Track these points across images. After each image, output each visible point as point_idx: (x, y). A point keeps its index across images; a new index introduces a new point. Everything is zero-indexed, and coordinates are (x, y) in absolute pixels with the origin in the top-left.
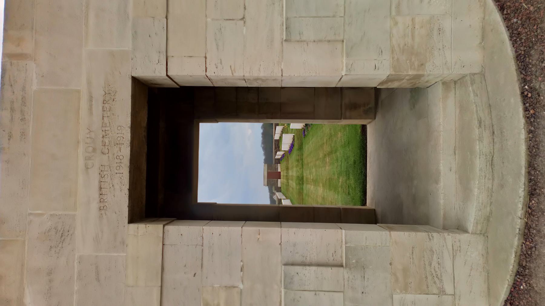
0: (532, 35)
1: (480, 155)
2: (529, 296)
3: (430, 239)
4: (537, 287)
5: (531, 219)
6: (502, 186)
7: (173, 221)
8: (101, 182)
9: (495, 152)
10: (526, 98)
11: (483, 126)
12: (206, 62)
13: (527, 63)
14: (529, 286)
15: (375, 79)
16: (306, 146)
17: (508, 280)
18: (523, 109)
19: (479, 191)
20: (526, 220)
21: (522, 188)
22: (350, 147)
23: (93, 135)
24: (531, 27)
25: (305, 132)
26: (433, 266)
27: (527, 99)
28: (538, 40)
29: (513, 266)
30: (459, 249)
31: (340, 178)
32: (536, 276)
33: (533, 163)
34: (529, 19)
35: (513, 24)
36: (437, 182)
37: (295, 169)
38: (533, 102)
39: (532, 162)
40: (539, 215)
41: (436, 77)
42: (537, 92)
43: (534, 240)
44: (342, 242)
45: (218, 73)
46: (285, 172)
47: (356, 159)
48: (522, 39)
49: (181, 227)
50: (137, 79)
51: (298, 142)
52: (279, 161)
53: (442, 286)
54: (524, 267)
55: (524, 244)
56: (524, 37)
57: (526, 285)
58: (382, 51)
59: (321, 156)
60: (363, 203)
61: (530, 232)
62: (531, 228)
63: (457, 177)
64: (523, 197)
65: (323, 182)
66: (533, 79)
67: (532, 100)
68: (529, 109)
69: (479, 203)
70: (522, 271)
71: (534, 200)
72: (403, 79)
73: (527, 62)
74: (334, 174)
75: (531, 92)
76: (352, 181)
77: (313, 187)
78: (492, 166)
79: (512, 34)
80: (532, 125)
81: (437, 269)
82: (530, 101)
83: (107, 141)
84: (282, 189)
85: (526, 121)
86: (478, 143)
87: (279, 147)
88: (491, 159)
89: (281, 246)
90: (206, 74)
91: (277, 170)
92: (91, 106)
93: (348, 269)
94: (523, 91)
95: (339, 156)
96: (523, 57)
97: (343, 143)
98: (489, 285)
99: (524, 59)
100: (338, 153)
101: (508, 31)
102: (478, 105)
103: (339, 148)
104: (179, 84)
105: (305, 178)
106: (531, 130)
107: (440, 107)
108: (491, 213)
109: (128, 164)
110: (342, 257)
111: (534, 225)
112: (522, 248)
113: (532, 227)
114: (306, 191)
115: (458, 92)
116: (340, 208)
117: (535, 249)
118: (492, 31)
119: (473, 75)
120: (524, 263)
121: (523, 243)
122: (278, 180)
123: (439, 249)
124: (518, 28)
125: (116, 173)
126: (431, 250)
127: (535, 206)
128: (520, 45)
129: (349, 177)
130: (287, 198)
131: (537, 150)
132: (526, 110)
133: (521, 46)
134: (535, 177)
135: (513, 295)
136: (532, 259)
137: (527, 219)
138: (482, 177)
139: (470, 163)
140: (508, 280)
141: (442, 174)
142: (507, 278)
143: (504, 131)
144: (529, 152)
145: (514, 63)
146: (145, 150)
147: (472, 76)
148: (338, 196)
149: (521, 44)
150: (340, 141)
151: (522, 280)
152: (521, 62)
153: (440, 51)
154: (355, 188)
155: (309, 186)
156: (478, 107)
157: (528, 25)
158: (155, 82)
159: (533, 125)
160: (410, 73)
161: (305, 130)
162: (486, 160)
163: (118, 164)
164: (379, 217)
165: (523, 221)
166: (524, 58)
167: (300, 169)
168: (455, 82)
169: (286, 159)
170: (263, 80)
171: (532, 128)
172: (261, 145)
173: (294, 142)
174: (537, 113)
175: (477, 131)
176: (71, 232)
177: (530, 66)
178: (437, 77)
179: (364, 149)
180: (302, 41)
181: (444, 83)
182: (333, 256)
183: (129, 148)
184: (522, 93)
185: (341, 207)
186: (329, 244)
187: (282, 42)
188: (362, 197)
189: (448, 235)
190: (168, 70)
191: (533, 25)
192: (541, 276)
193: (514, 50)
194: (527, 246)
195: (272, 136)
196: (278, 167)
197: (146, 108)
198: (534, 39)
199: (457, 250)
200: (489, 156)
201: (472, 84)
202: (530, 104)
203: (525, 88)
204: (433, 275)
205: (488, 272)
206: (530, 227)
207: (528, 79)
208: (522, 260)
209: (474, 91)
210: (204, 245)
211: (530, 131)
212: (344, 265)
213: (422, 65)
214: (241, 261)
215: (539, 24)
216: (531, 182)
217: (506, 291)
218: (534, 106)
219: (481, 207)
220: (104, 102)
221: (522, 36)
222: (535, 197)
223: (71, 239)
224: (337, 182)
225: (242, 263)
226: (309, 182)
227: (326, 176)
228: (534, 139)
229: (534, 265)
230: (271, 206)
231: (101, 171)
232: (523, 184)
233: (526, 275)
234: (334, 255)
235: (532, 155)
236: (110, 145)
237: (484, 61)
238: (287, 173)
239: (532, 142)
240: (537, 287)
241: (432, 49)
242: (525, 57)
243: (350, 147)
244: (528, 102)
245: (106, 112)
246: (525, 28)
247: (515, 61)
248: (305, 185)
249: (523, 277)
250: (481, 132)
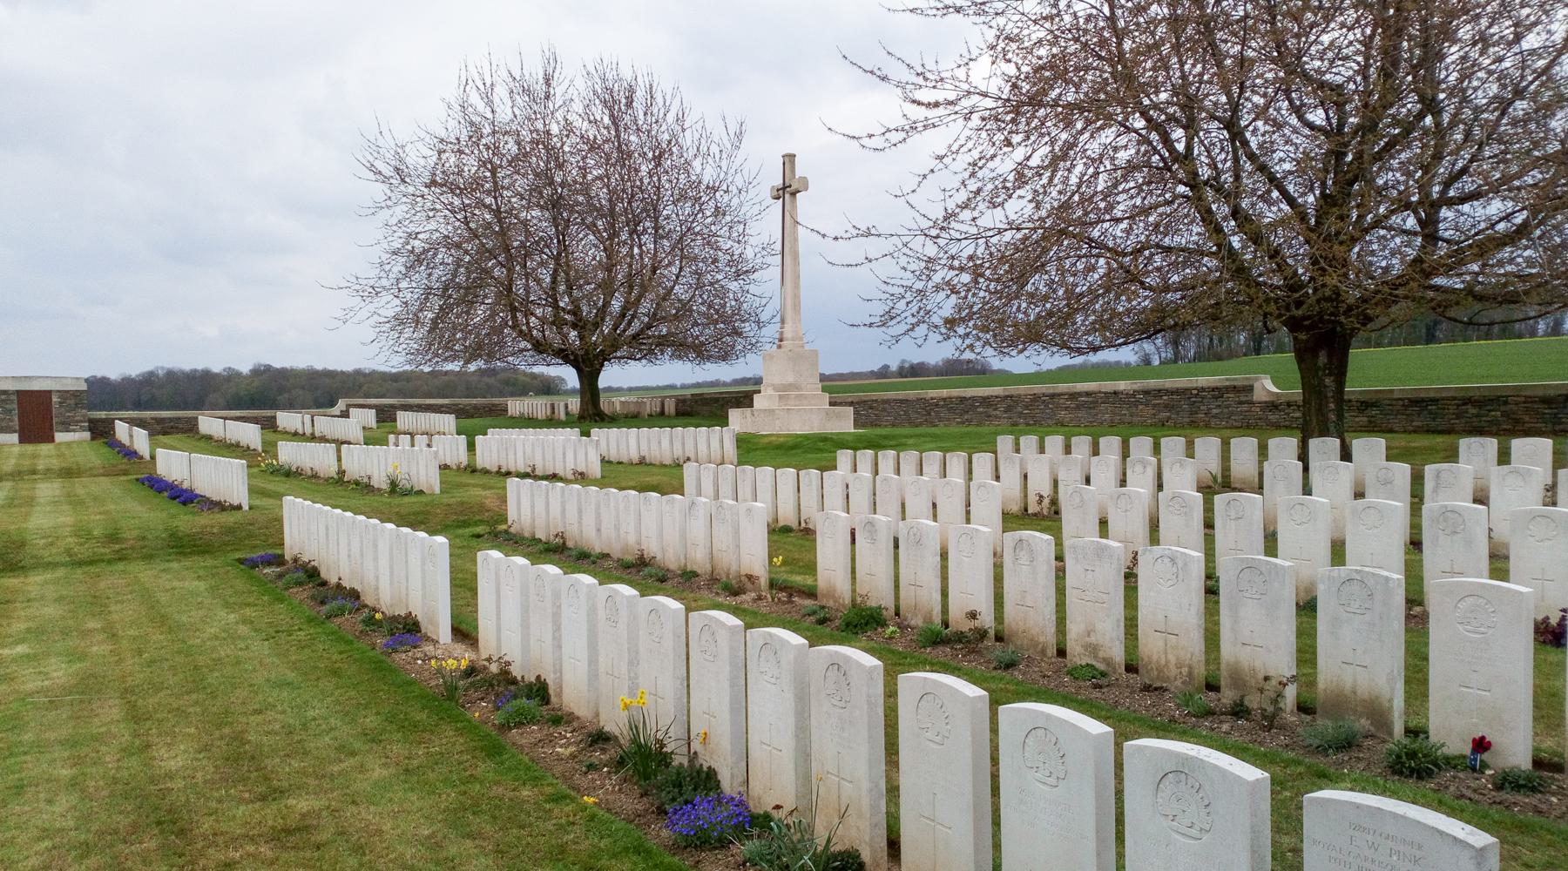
46: (55, 463)
51: (215, 531)
52: (101, 431)
122: (15, 432)
167: (68, 552)
169: (114, 466)
172: (162, 368)
196: (74, 431)
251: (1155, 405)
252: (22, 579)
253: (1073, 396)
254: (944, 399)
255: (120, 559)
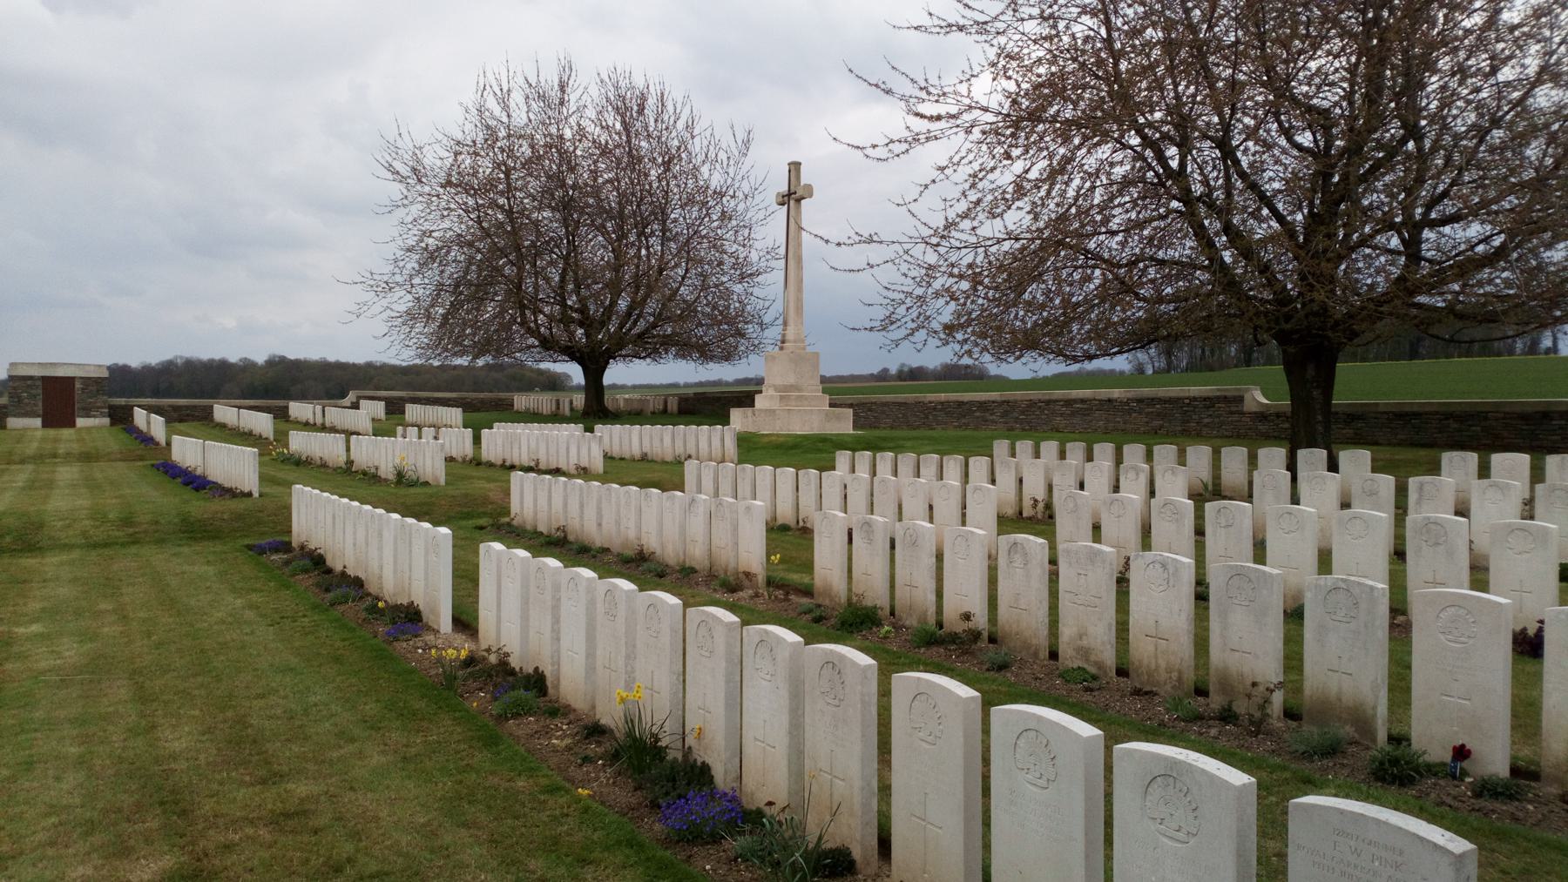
46: (76, 448)
51: (225, 517)
52: (121, 417)
105: (29, 562)
122: (39, 416)
172: (181, 357)
173: (227, 496)
196: (94, 416)
238: (69, 457)
251: (1148, 414)
253: (1069, 403)
254: (942, 403)
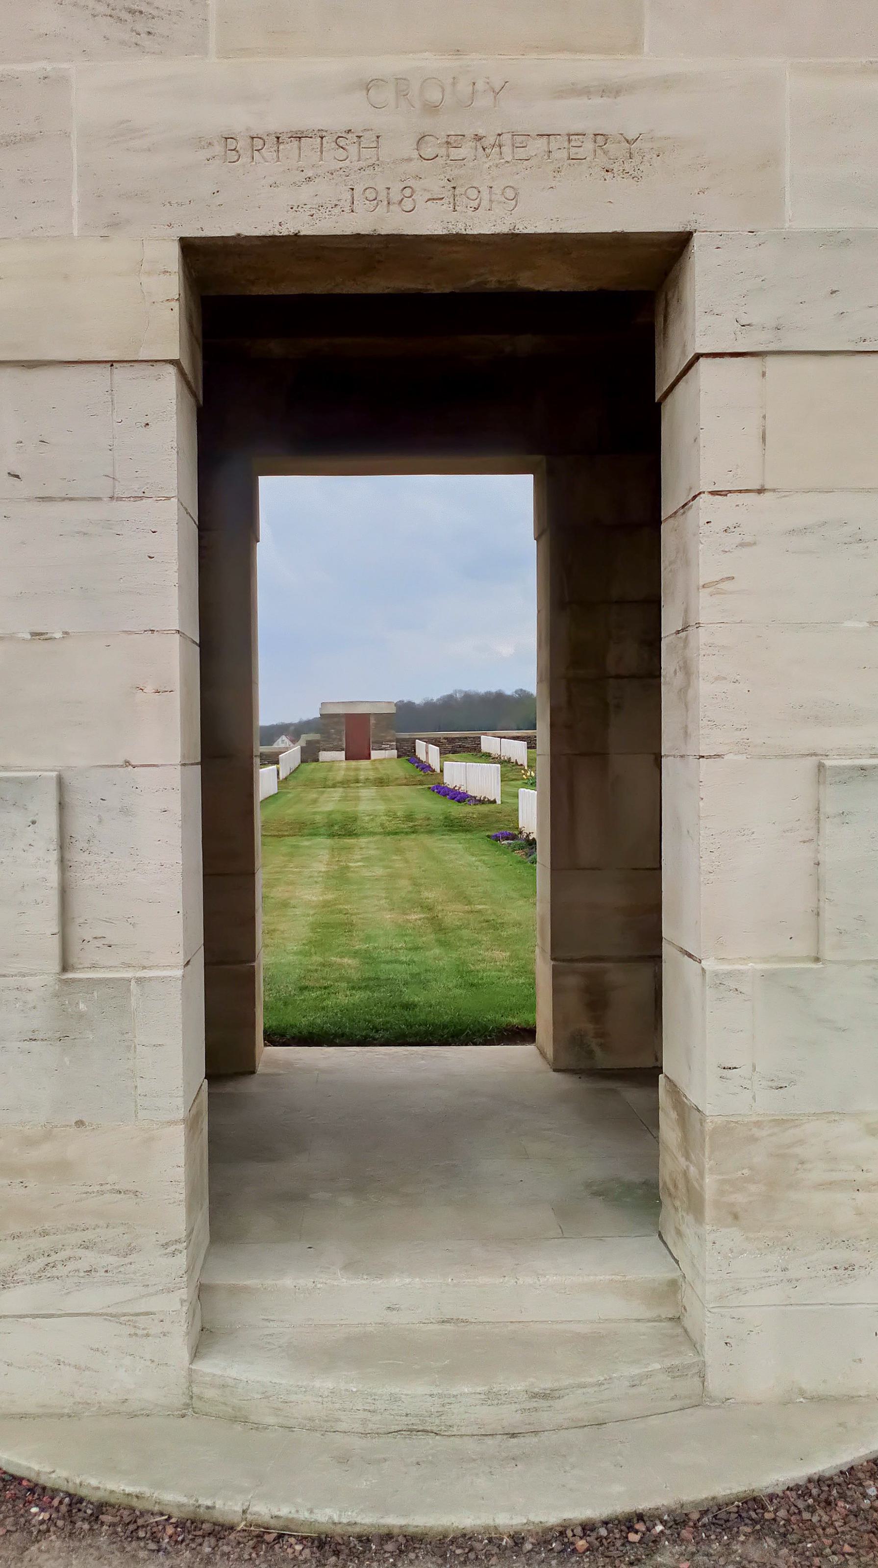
0: (824, 1540)
1: (440, 1396)
2: (9, 1528)
3: (165, 1245)
4: (40, 1550)
5: (245, 1540)
6: (343, 1459)
7: (194, 394)
8: (322, 138)
9: (452, 1438)
10: (623, 1528)
11: (535, 1405)
12: (747, 491)
13: (735, 1529)
14: (39, 1531)
15: (690, 1069)
16: (460, 843)
17: (54, 1472)
18: (590, 1519)
19: (326, 1393)
20: (242, 1526)
21: (340, 1516)
22: (458, 991)
23: (484, 101)
24: (848, 1537)
25: (507, 839)
26: (81, 1252)
27: (621, 1531)
28: (808, 1557)
29: (98, 1488)
30: (140, 1332)
31: (354, 958)
32: (72, 1551)
33: (420, 1548)
34: (874, 1529)
35: (861, 1485)
36: (351, 1267)
37: (381, 807)
38: (611, 1548)
39: (423, 1546)
40: (257, 1562)
41: (695, 1261)
42: (644, 1557)
43: (179, 1547)
44: (144, 968)
45: (708, 537)
46: (372, 775)
47: (421, 1011)
48: (813, 1512)
49: (174, 422)
50: (666, 273)
51: (475, 816)
52: (407, 752)
53: (22, 1281)
54: (97, 1517)
55: (166, 1520)
56: (819, 1518)
57: (42, 1522)
58: (781, 1087)
59: (426, 894)
60: (275, 1034)
61: (204, 1537)
62: (218, 1541)
63: (370, 1329)
64: (313, 1520)
65: (341, 904)
66: (684, 1547)
67: (618, 1543)
68: (589, 1536)
69: (288, 1392)
70: (85, 1512)
71: (303, 1549)
72: (688, 1157)
73: (738, 1528)
74: (368, 938)
75: (645, 1540)
76: (343, 998)
77: (323, 870)
78: (409, 1433)
79: (829, 1482)
80: (539, 1544)
81: (71, 1266)
82: (615, 1539)
83: (466, 150)
84: (313, 765)
85: (551, 1529)
86: (479, 1390)
87: (454, 752)
88: (429, 1428)
89: (122, 766)
90: (704, 492)
91: (376, 746)
92: (586, 92)
93: (57, 987)
94: (645, 1518)
95: (427, 953)
96: (754, 1515)
97: (472, 968)
98: (35, 1417)
99: (747, 1521)
100: (437, 951)
101: (838, 1471)
102: (603, 1387)
103: (454, 955)
104: (669, 399)
106: (522, 1543)
107: (596, 1275)
108: (257, 1429)
109: (385, 229)
110: (93, 967)
111: (226, 1549)
112: (152, 1514)
113: (220, 1543)
114: (309, 847)
115: (643, 1327)
116: (254, 961)
117: (154, 1551)
118: (840, 1425)
119: (700, 1372)
120: (110, 1517)
121: (170, 1518)
122: (342, 750)
123: (135, 1273)
124: (846, 1501)
125: (353, 189)
126: (130, 1250)
127: (285, 1551)
128: (793, 1508)
129: (360, 988)
130: (283, 783)
131: (462, 1559)
132: (587, 1528)
133: (788, 1512)
134: (375, 1553)
135: (11, 1485)
136: (121, 1541)
137: (245, 1528)
138: (370, 1401)
139: (416, 1367)
140: (54, 1472)
141: (375, 1282)
142: (58, 1470)
143: (519, 1467)
144: (454, 1538)
145: (734, 1491)
146: (436, 286)
147: (695, 1370)
148: (295, 953)
149: (797, 1511)
150: (480, 958)
151: (57, 1510)
152: (737, 1512)
153: (779, 1269)
154: (323, 1008)
155: (325, 855)
156: (596, 1389)
157: (855, 1528)
158: (672, 316)
159: (538, 1547)
160: (707, 1180)
161: (513, 839)
162: (426, 1414)
163: (383, 195)
164: (230, 1087)
165: (236, 1519)
166: (752, 1520)
167: (382, 825)
168: (679, 1318)
169: (413, 777)
170: (683, 691)
171: (528, 1546)
172: (460, 691)
174: (574, 1559)
175: (518, 1386)
176: (146, 41)
177: (726, 1538)
178: (694, 1265)
179: (453, 1037)
180: (818, 821)
181: (673, 1286)
182: (96, 938)
183: (440, 231)
184: (640, 1517)
185: (259, 964)
186: (134, 925)
187: (815, 755)
188: (295, 1030)
189: (182, 1301)
190: (718, 360)
191: (854, 1543)
192: (74, 1562)
193: (779, 1491)
194: (160, 1527)
195: (490, 728)
196: (385, 749)
197: (583, 287)
198: (809, 1545)
199: (135, 1327)
200: (437, 1422)
201: (670, 1370)
202: (606, 1538)
203: (654, 1526)
204: (52, 1253)
205: (74, 1416)
206: (220, 1538)
207: (683, 1531)
208: (118, 1514)
209: (649, 1375)
210: (114, 503)
211: (521, 1541)
212: (70, 975)
213: (736, 1217)
214: (66, 633)
215: (858, 1558)
216: (361, 1541)
217: (19, 1466)
218: (597, 1549)
219: (275, 1397)
220: (599, 137)
221: (821, 1512)
222: (312, 1553)
223: (123, 43)
224: (340, 949)
225: (58, 635)
226: (339, 854)
227: (359, 914)
228: (495, 1550)
229: (105, 1546)
230: (254, 730)
231: (359, 137)
232: (353, 1520)
233: (71, 1522)
234: (99, 943)
235: (445, 1545)
236: (448, 162)
237: (744, 1403)
239: (486, 1545)
240: (40, 1550)
241: (785, 1248)
242: (755, 1522)
243: (458, 991)
244: (613, 1532)
245: (566, 144)
246: (847, 1520)
247: (742, 1495)
248: (329, 842)
249: (67, 1514)
250: (516, 1400)
252: (356, 840)
255: (413, 832)
